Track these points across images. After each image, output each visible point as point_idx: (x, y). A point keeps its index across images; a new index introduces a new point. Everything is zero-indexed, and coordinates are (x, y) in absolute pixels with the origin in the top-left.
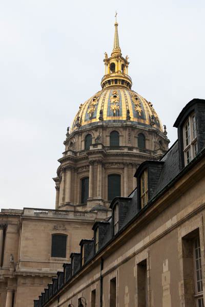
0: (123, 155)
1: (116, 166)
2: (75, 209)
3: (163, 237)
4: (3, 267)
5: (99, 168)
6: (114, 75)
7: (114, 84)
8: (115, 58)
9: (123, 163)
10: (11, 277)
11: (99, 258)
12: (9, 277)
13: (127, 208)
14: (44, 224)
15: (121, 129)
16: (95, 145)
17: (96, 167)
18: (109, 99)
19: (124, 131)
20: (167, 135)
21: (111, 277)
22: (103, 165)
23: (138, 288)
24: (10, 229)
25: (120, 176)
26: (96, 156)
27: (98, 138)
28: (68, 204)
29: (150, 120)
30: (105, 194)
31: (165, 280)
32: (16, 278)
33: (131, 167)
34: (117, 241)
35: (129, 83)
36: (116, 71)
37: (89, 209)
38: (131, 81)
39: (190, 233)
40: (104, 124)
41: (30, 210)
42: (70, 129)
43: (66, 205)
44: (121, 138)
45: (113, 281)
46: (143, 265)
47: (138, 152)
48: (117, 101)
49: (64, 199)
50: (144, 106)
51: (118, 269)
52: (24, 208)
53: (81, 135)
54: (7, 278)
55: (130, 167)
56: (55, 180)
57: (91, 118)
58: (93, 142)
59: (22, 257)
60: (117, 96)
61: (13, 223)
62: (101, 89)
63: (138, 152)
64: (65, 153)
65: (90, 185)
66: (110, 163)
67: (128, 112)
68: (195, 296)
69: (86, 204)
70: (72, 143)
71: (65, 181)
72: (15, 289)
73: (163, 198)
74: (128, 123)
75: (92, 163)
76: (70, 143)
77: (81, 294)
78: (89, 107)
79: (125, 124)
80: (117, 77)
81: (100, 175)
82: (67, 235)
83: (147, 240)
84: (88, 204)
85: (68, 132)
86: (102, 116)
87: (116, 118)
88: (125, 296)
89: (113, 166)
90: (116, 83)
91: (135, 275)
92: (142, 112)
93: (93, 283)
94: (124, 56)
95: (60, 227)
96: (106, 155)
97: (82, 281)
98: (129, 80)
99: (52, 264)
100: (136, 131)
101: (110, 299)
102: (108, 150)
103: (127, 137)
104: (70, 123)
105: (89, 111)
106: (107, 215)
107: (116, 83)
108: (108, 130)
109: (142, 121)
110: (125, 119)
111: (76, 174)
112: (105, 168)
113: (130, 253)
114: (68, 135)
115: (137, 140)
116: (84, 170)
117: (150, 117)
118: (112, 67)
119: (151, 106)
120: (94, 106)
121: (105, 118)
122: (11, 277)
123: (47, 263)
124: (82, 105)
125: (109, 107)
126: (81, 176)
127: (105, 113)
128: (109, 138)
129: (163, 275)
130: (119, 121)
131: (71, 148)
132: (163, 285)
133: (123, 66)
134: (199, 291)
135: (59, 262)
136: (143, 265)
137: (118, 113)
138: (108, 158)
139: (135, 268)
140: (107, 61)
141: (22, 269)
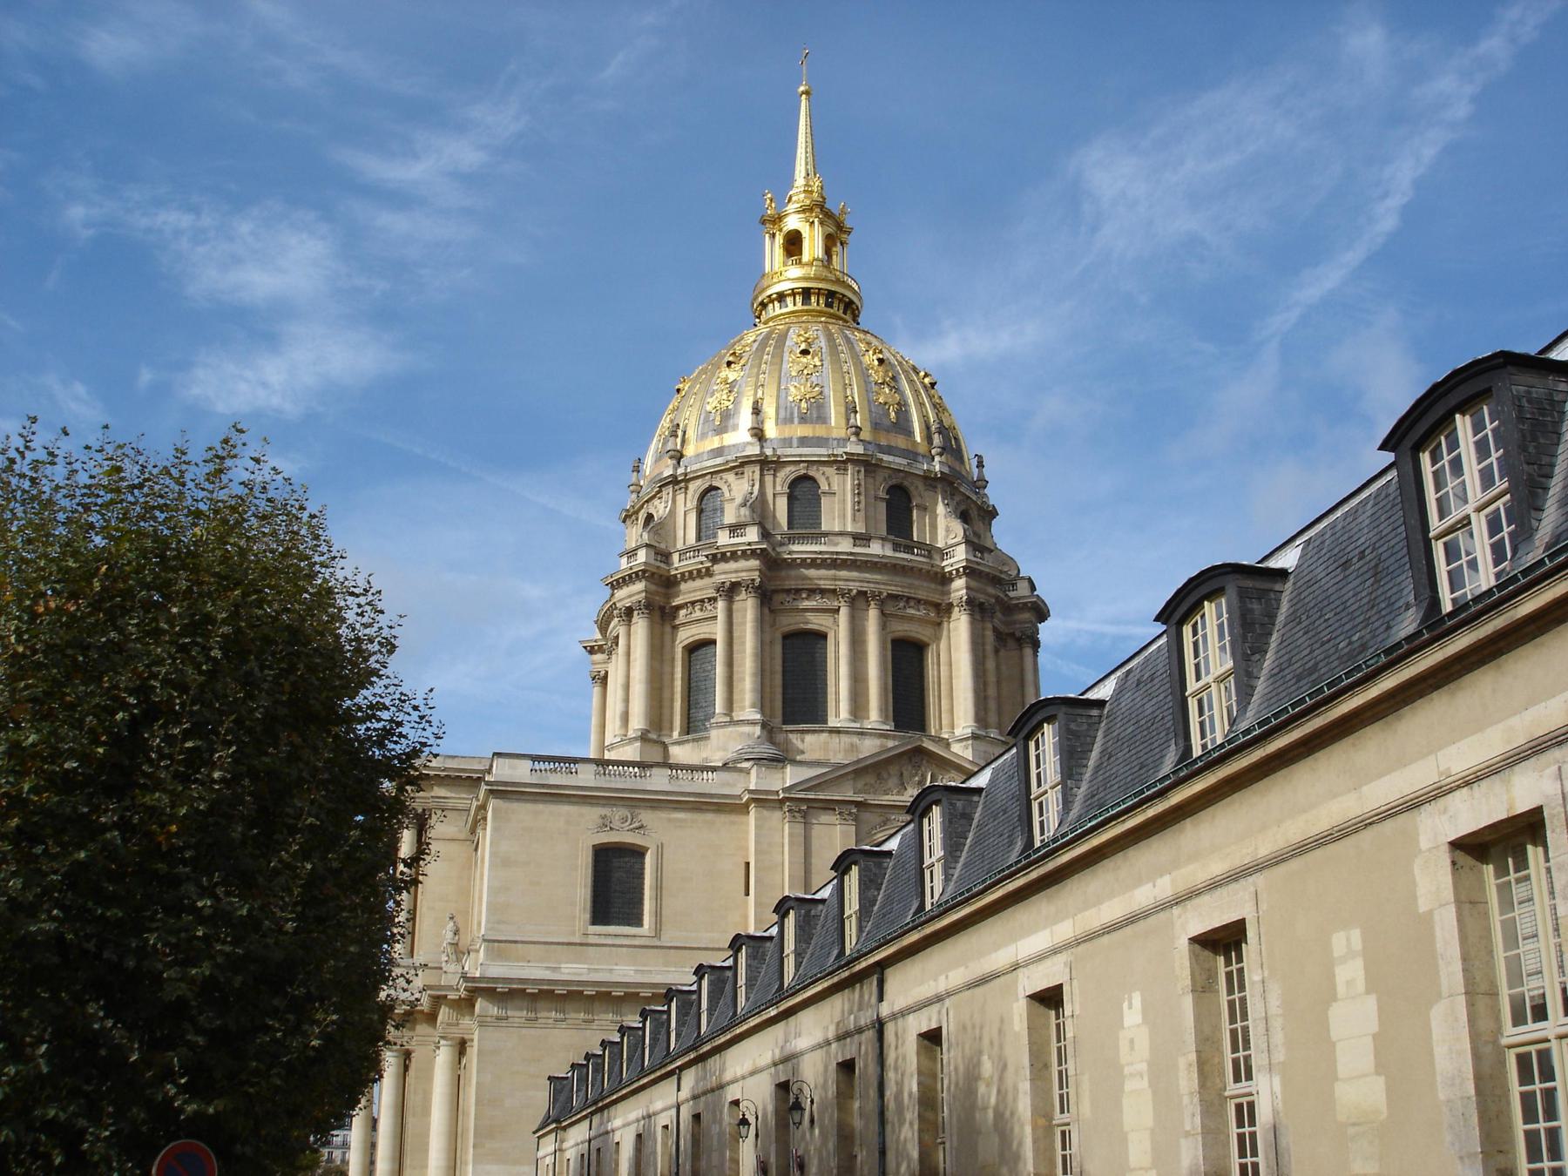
14: (565, 809)
25: (824, 636)
31: (1132, 1048)
35: (851, 302)
38: (860, 299)
40: (769, 452)
47: (889, 552)
57: (721, 430)
63: (889, 552)
65: (720, 670)
66: (788, 591)
76: (642, 515)
83: (1066, 930)
84: (714, 733)
87: (801, 431)
90: (806, 300)
91: (1017, 1028)
100: (881, 475)
109: (900, 442)
112: (771, 611)
113: (1000, 959)
119: (933, 385)
121: (771, 431)
122: (452, 996)
126: (685, 636)
127: (769, 409)
129: (1124, 1036)
132: (1123, 1061)
138: (783, 573)
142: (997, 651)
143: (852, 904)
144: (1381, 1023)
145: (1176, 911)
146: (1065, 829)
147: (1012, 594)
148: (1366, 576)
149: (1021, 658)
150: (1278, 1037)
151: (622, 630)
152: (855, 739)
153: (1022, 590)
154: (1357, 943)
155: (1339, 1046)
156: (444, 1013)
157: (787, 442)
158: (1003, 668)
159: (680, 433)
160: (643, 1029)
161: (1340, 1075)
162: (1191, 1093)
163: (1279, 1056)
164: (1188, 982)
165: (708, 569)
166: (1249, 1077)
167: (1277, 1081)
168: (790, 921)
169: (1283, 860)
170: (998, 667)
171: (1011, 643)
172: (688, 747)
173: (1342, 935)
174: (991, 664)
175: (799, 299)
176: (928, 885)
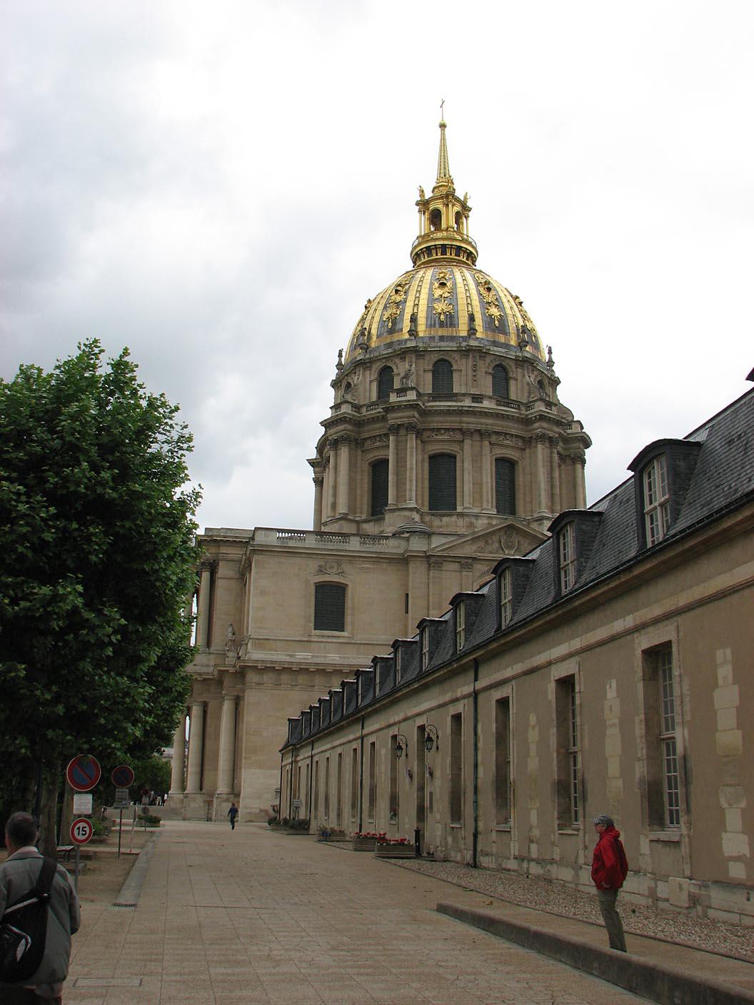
0: (461, 412)
1: (446, 437)
2: (358, 529)
3: (606, 643)
4: (213, 649)
5: (412, 441)
6: (439, 235)
7: (439, 256)
8: (442, 198)
9: (460, 430)
10: (232, 670)
11: (471, 660)
12: (228, 671)
13: (527, 577)
14: (298, 560)
15: (457, 356)
16: (402, 391)
17: (404, 438)
18: (431, 289)
19: (464, 360)
20: (554, 368)
21: (498, 694)
22: (419, 434)
23: (557, 719)
24: (223, 570)
25: (455, 457)
26: (400, 415)
27: (406, 376)
28: (344, 518)
29: (518, 336)
30: (422, 497)
31: (611, 710)
32: (241, 673)
33: (478, 438)
34: (512, 637)
35: (471, 253)
36: (444, 226)
37: (389, 530)
38: (477, 252)
39: (656, 646)
41: (268, 532)
42: (344, 354)
43: (340, 519)
44: (455, 375)
45: (503, 703)
46: (566, 684)
47: (495, 407)
48: (446, 295)
49: (334, 506)
50: (507, 305)
51: (513, 682)
52: (255, 528)
53: (370, 367)
54: (222, 673)
55: (476, 437)
56: (312, 463)
57: (391, 331)
58: (397, 385)
59: (252, 629)
60: (448, 284)
61: (230, 557)
62: (409, 265)
64: (336, 407)
65: (391, 477)
67: (472, 318)
68: (662, 737)
69: (384, 519)
70: (349, 385)
71: (336, 468)
72: (241, 695)
73: (608, 584)
74: (473, 343)
75: (396, 429)
77: (424, 717)
78: (385, 307)
79: (464, 344)
80: (443, 237)
81: (412, 455)
82: (347, 585)
83: (577, 644)
84: (387, 516)
85: (340, 360)
86: (416, 326)
87: (441, 332)
88: (530, 729)
89: (440, 437)
90: (444, 253)
91: (550, 697)
92: (502, 320)
93: (456, 700)
94: (460, 194)
95: (332, 568)
96: (424, 413)
97: (426, 695)
98: (473, 247)
99: (317, 644)
100: (488, 359)
101: (497, 732)
102: (429, 401)
103: (470, 373)
104: (343, 339)
105: (387, 315)
106: (429, 544)
107: (444, 253)
108: (427, 358)
109: (502, 339)
110: (464, 334)
111: (359, 452)
112: (422, 442)
114: (339, 366)
115: (490, 378)
116: (378, 443)
117: (518, 330)
118: (435, 218)
119: (521, 303)
120: (398, 304)
123: (306, 643)
124: (369, 301)
125: (430, 308)
127: (422, 320)
128: (431, 374)
130: (452, 338)
131: (349, 397)
133: (458, 217)
134: (667, 730)
135: (329, 640)
136: (566, 684)
137: (451, 320)
138: (429, 419)
139: (552, 687)
140: (423, 204)
141: (255, 655)
142: (560, 466)
143: (507, 597)
144: (741, 700)
145: (636, 635)
146: (577, 586)
147: (569, 431)
148: (740, 450)
149: (574, 470)
150: (687, 707)
151: (332, 454)
152: (473, 520)
153: (575, 429)
154: (729, 657)
155: (718, 714)
156: (227, 681)
157: (432, 338)
158: (563, 476)
159: (366, 333)
160: (343, 692)
161: (720, 728)
162: (641, 737)
163: (688, 718)
164: (641, 674)
165: (383, 416)
166: (673, 729)
167: (686, 731)
168: (508, 581)
169: (693, 609)
170: (560, 475)
171: (568, 461)
172: (372, 524)
173: (722, 651)
174: (556, 474)
175: (439, 251)
176: (503, 615)
